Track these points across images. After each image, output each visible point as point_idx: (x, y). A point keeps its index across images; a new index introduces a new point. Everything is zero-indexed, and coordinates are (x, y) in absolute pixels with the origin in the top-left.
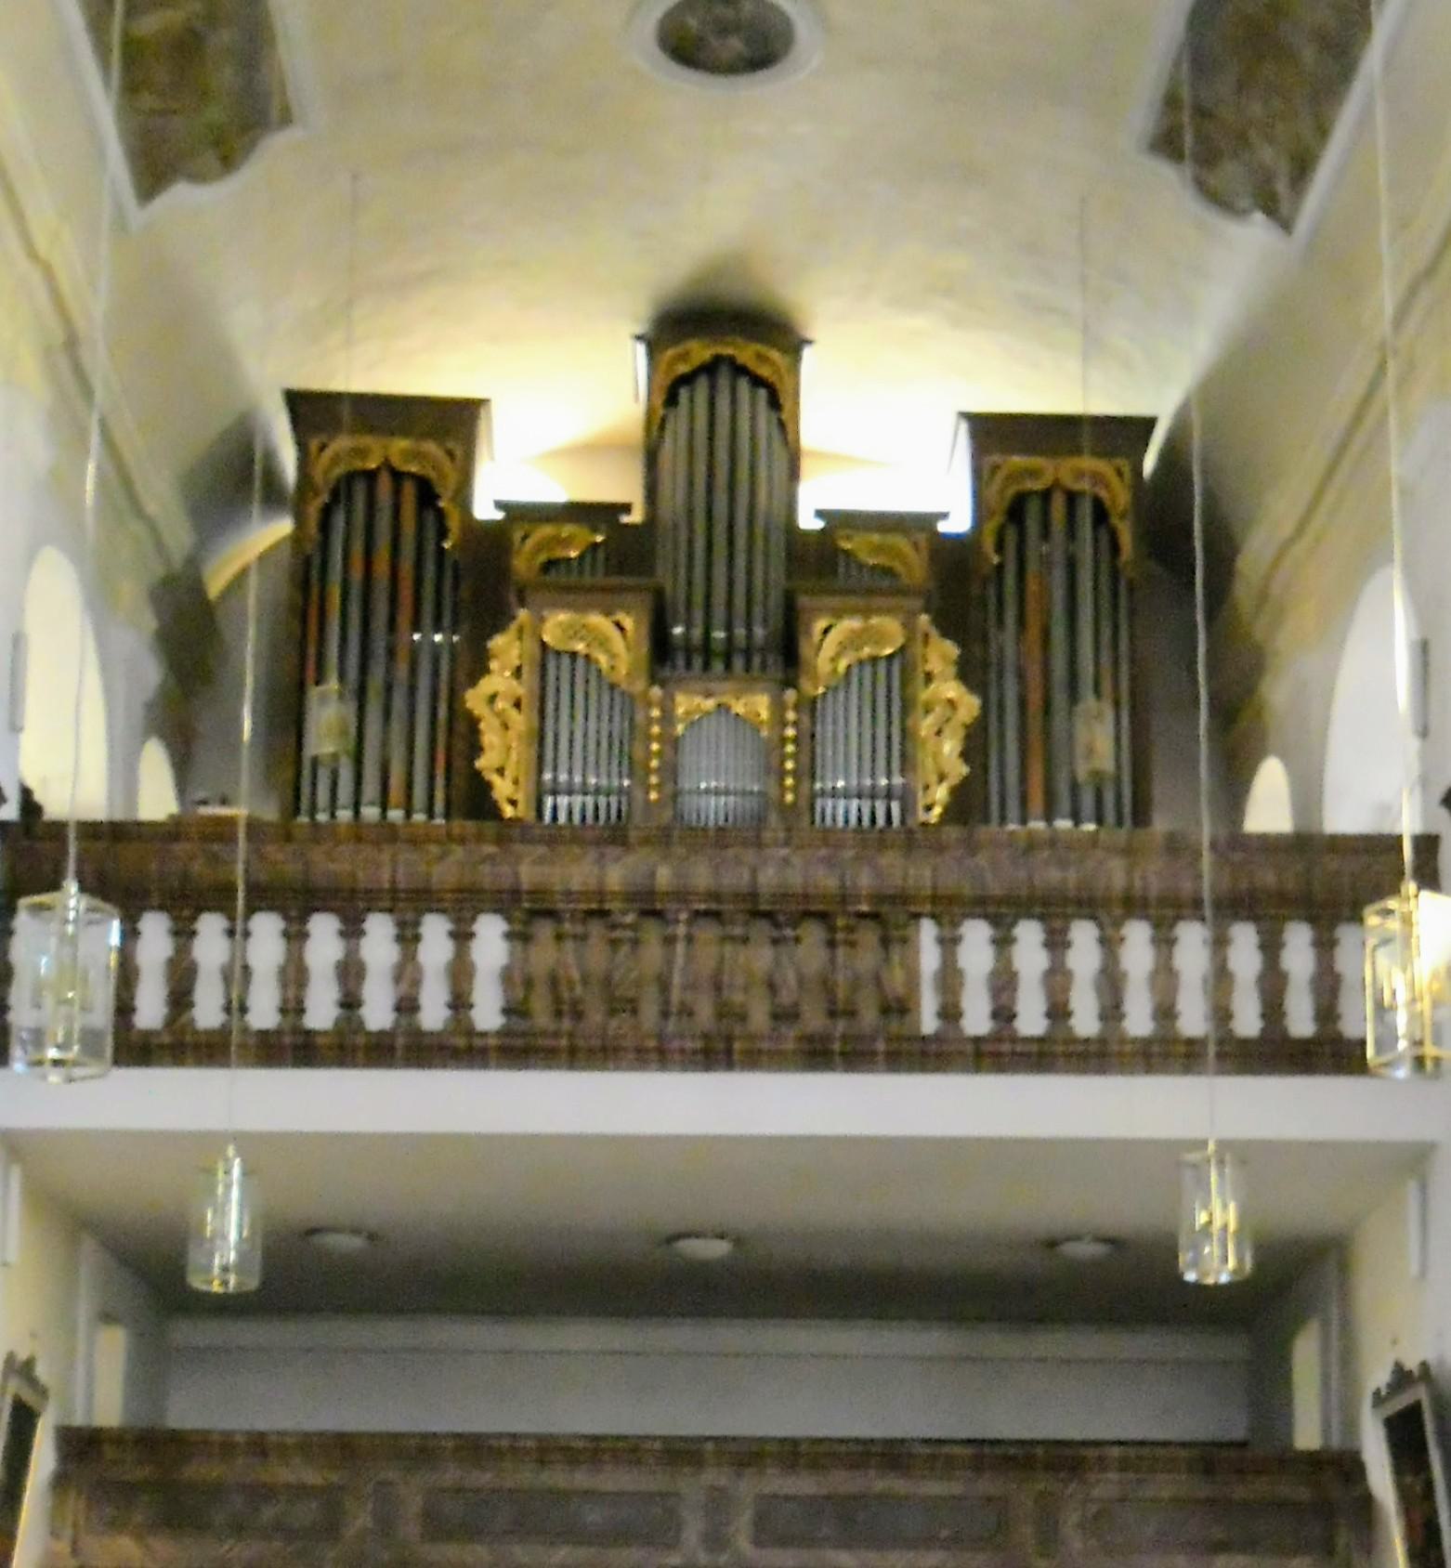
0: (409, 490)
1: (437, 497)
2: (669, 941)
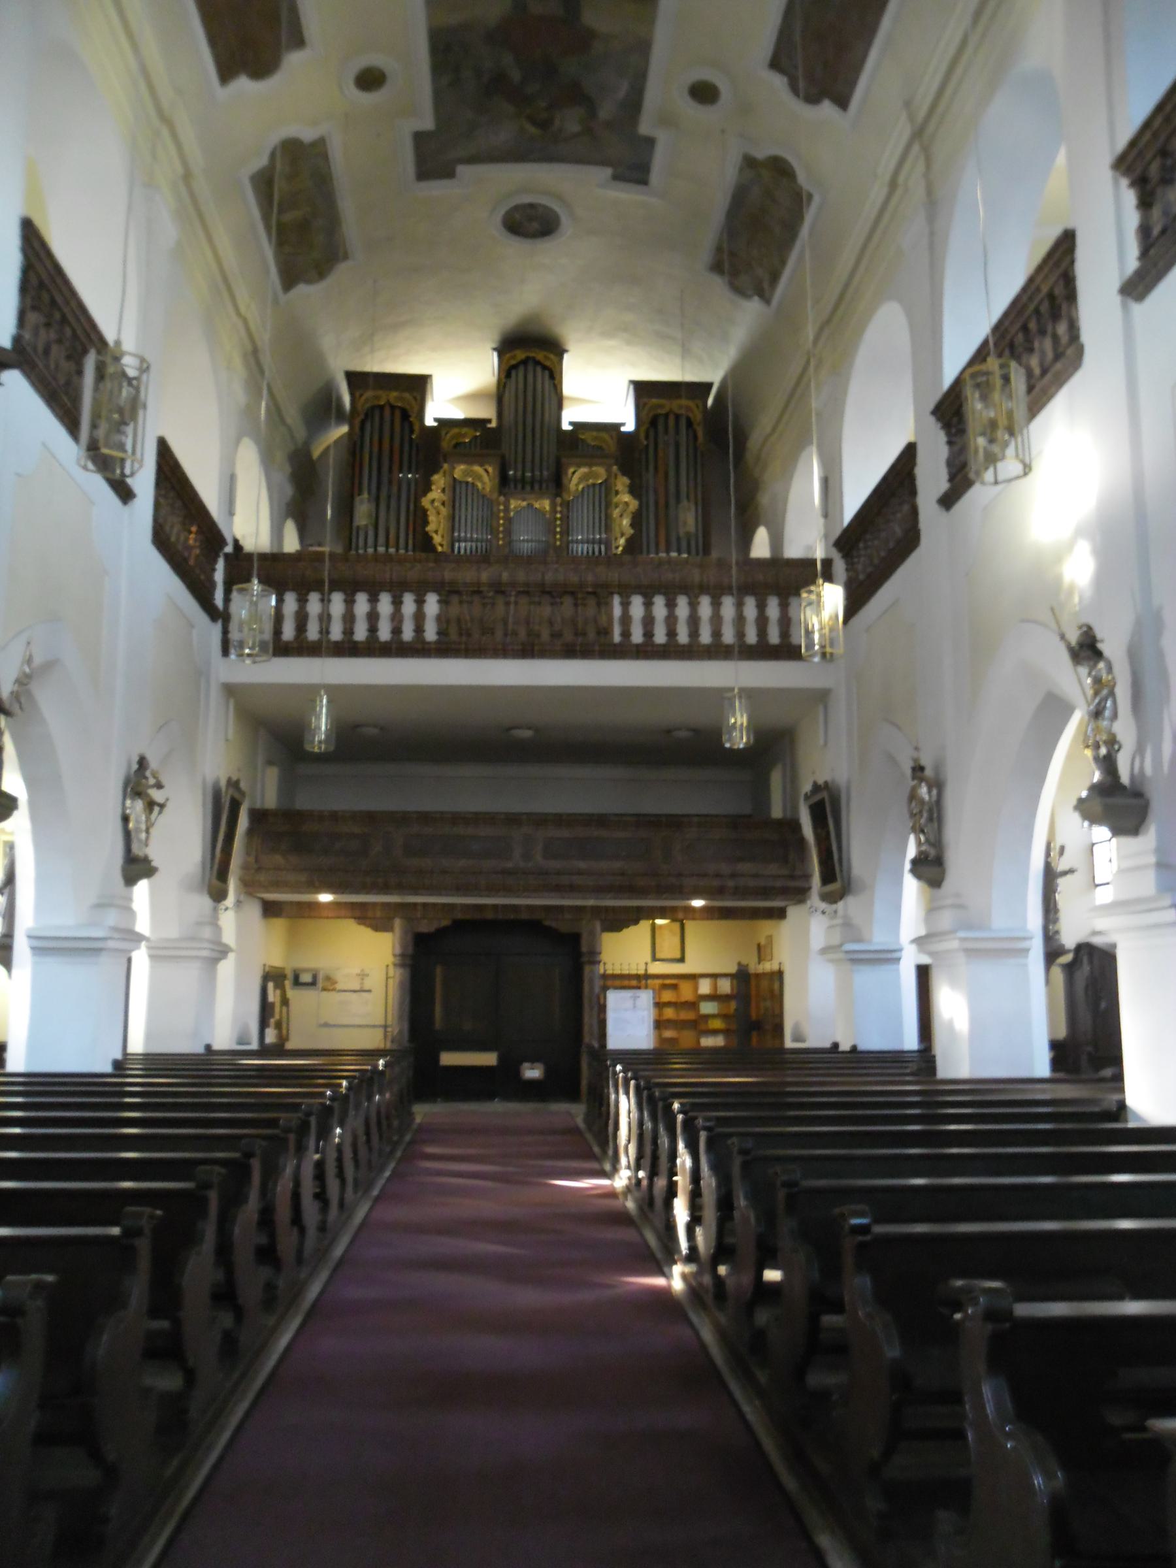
0: (398, 414)
1: (410, 416)
2: (507, 604)
